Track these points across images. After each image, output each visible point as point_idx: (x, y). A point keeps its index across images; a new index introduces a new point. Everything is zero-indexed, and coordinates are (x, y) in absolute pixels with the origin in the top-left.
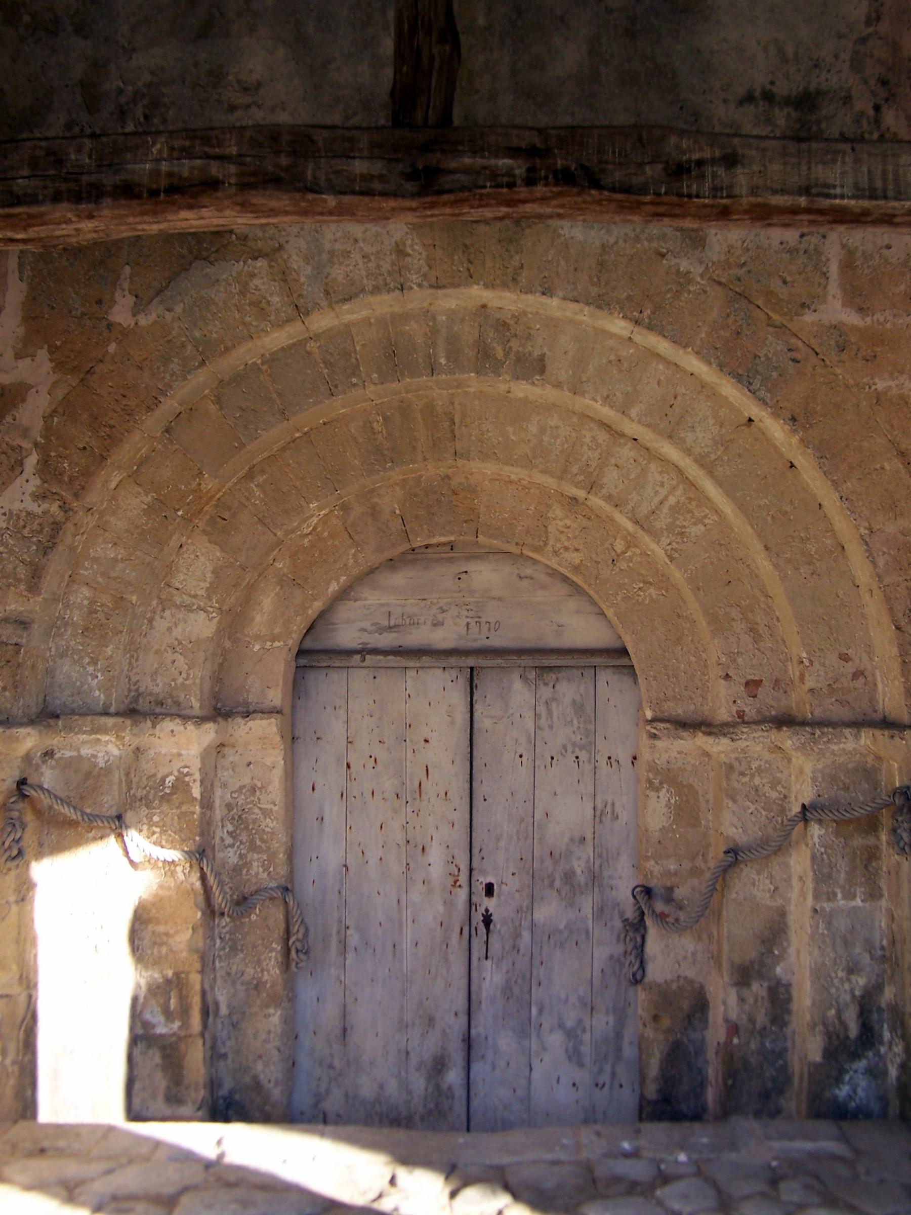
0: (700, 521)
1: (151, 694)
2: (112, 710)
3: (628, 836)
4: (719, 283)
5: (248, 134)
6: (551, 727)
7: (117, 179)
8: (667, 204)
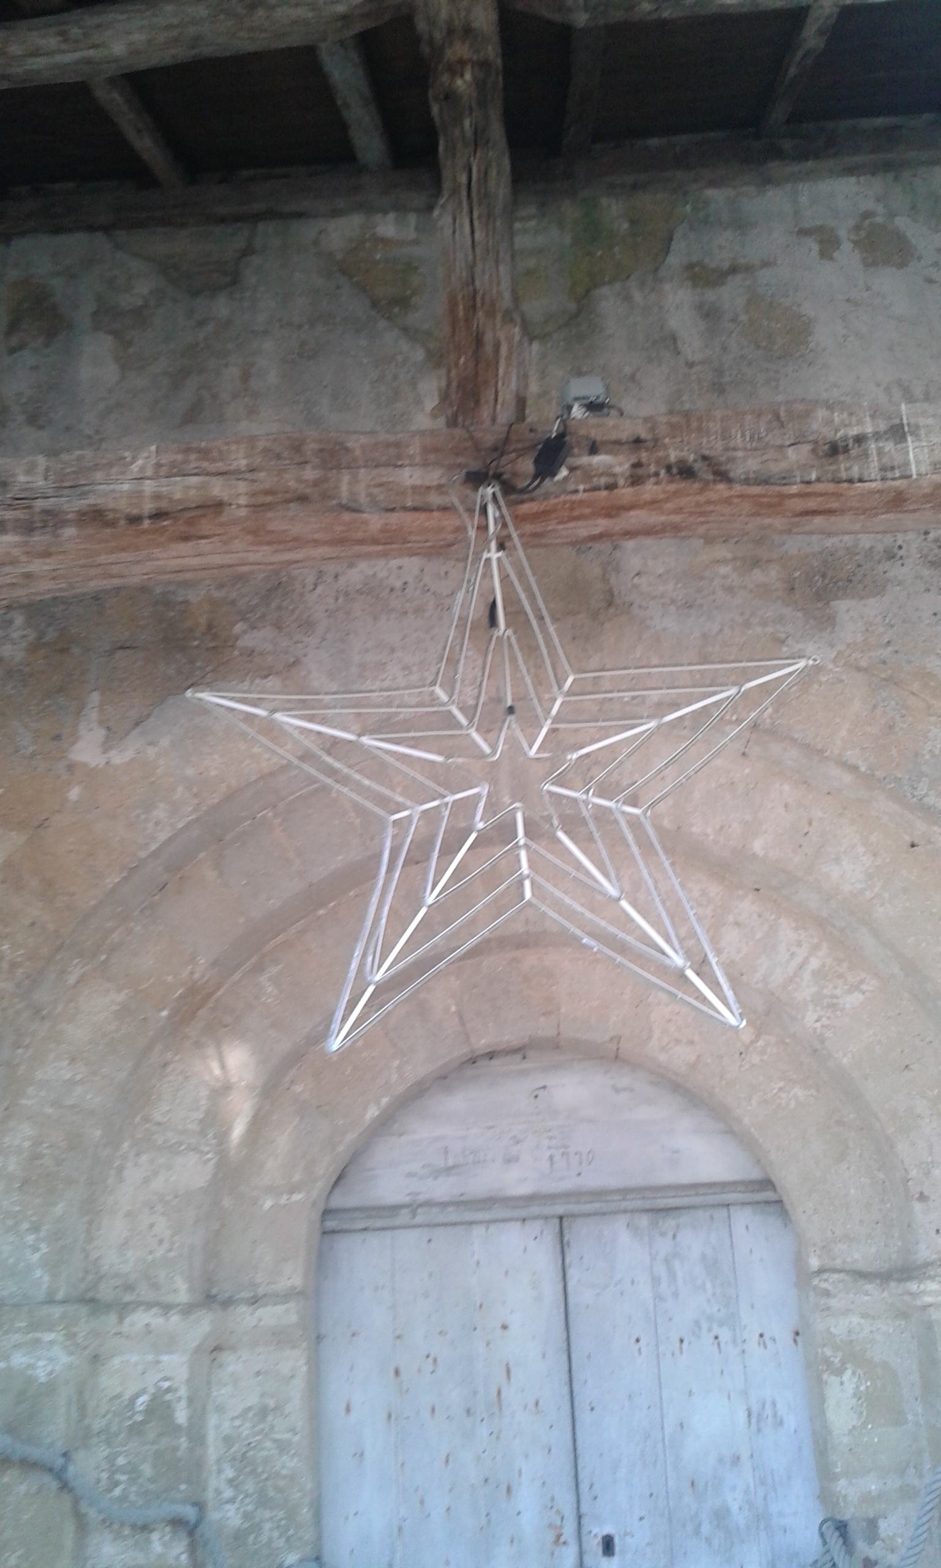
0: (855, 988)
1: (117, 1275)
2: (60, 1296)
3: (800, 1449)
4: (858, 669)
5: (261, 444)
6: (676, 1295)
7: (83, 504)
8: (821, 495)
